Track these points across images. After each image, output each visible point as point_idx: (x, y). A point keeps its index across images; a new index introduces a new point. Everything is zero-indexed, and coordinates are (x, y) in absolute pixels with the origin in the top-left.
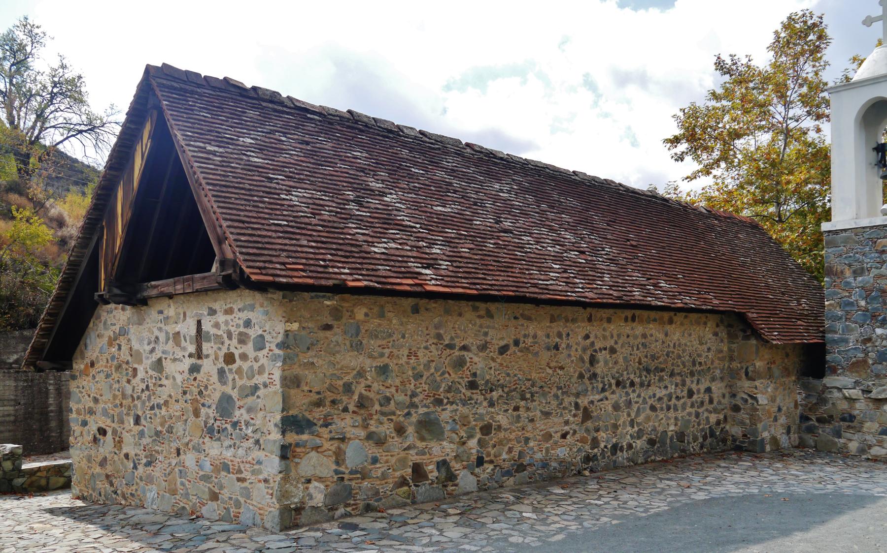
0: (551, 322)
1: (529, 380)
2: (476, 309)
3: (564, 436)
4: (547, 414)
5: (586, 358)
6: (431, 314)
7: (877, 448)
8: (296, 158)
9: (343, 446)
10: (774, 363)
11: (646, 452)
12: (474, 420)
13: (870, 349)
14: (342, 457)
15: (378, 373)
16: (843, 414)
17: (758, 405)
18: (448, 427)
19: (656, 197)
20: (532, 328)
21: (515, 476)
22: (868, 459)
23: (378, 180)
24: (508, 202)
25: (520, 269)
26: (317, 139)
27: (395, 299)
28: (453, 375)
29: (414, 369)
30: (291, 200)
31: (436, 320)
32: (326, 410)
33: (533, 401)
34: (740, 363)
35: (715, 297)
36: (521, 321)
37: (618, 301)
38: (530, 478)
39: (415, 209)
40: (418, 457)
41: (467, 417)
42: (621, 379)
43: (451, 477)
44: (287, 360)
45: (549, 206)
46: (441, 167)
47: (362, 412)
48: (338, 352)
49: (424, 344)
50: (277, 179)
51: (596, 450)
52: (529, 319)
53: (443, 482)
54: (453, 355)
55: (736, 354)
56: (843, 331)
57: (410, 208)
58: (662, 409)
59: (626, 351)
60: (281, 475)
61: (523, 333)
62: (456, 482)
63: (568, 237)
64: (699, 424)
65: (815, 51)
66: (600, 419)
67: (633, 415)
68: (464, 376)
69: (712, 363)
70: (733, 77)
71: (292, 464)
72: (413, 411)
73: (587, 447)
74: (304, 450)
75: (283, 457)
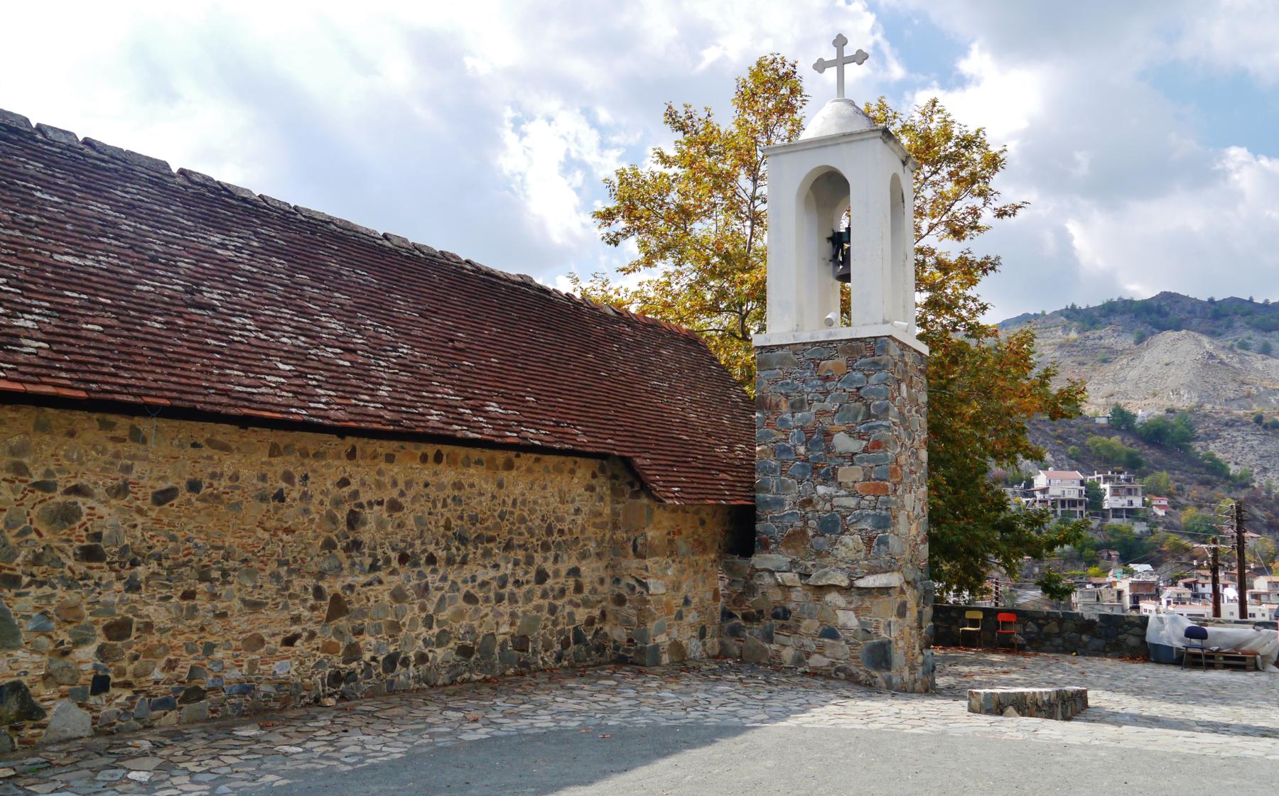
0: (270, 456)
3: (289, 641)
4: (255, 606)
5: (342, 516)
7: (817, 657)
10: (680, 532)
11: (454, 667)
12: (91, 614)
13: (810, 515)
16: (776, 607)
17: (648, 594)
18: (29, 625)
19: (529, 286)
20: (228, 464)
22: (805, 673)
33: (225, 583)
34: (626, 532)
35: (585, 433)
37: (392, 427)
38: (213, 712)
39: (9, 254)
41: (76, 607)
42: (409, 552)
45: (312, 279)
46: (106, 198)
51: (354, 665)
52: (225, 448)
55: (621, 518)
56: (777, 490)
58: (487, 600)
59: (422, 508)
61: (210, 470)
62: (43, 721)
63: (333, 326)
64: (555, 623)
65: (786, 108)
66: (364, 615)
67: (431, 609)
68: (73, 538)
69: (583, 531)
70: (687, 136)
73: (337, 660)
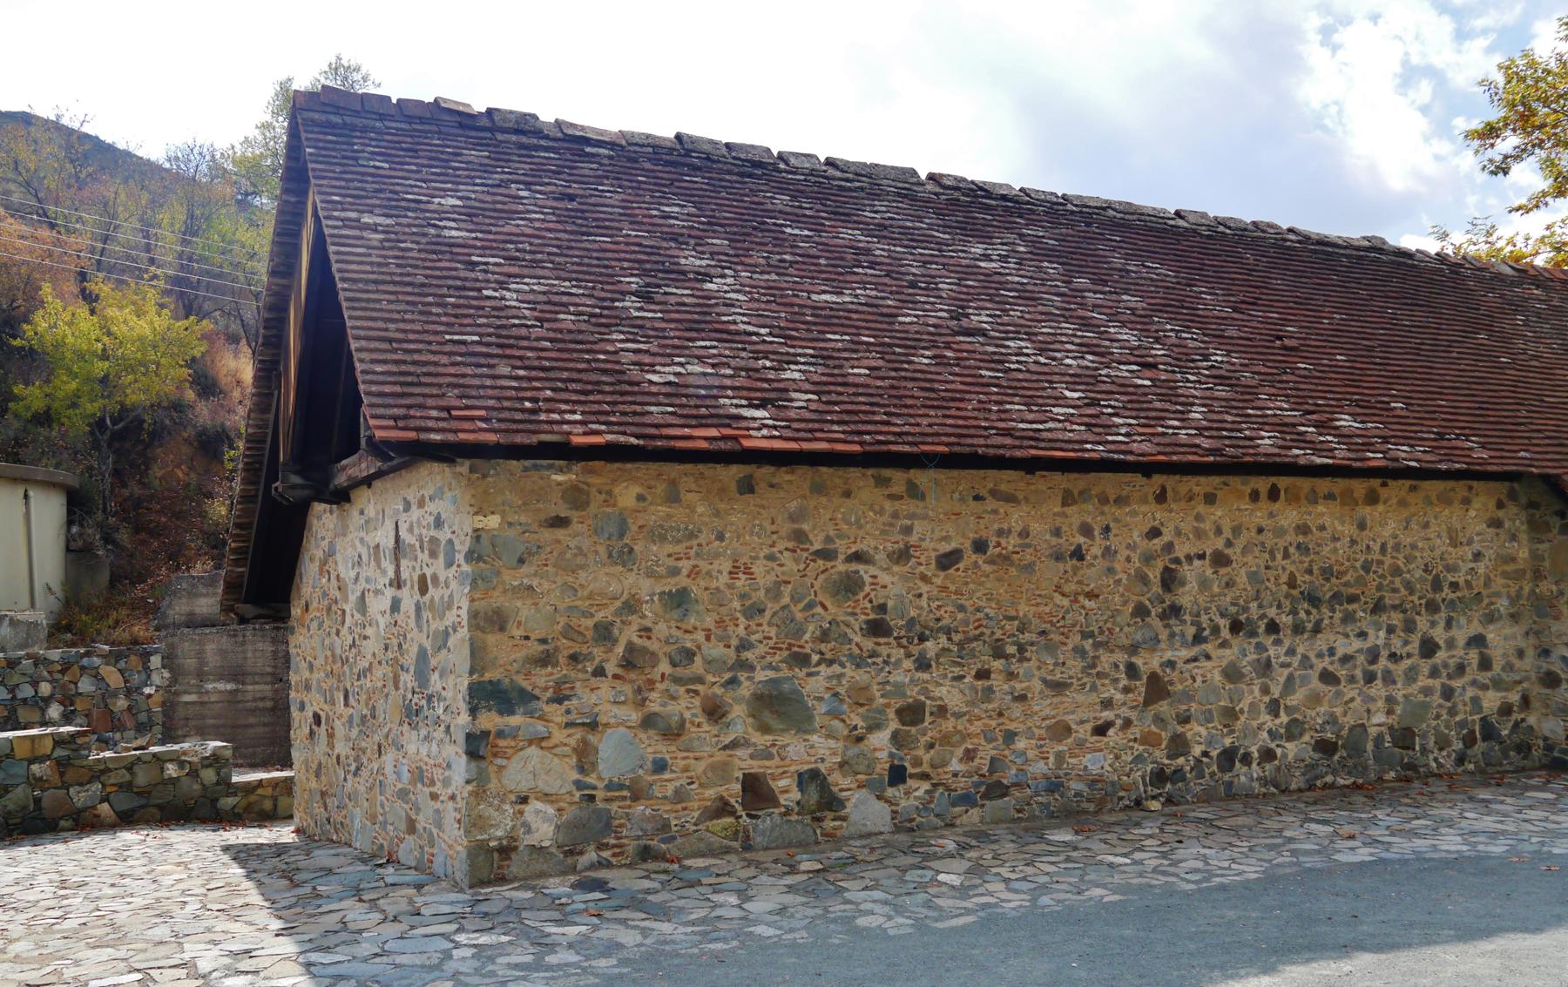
0: (1064, 504)
1: (1012, 619)
2: (882, 482)
3: (1101, 730)
4: (1058, 687)
5: (1154, 574)
6: (782, 494)
8: (537, 225)
9: (592, 738)
11: (1311, 767)
12: (882, 696)
14: (592, 758)
15: (665, 605)
18: (822, 708)
19: (1380, 250)
20: (1016, 517)
21: (983, 806)
23: (703, 253)
24: (997, 278)
25: (980, 402)
26: (596, 190)
27: (701, 467)
28: (832, 609)
29: (743, 597)
30: (503, 298)
31: (793, 505)
32: (562, 670)
33: (1022, 660)
34: (1556, 583)
35: (1483, 446)
36: (991, 504)
37: (1212, 458)
38: (1019, 811)
40: (755, 763)
41: (867, 688)
42: (1243, 618)
43: (831, 803)
44: (480, 582)
45: (1094, 282)
47: (633, 675)
48: (581, 567)
49: (766, 551)
50: (486, 264)
51: (1181, 760)
52: (1011, 499)
53: (813, 812)
54: (833, 571)
55: (1547, 564)
57: (758, 301)
59: (1256, 561)
60: (470, 788)
61: (996, 526)
62: (842, 813)
63: (1125, 337)
64: (1452, 712)
66: (1191, 698)
67: (1276, 691)
71: (492, 769)
72: (742, 676)
73: (1160, 754)
74: (513, 744)
75: (473, 754)
